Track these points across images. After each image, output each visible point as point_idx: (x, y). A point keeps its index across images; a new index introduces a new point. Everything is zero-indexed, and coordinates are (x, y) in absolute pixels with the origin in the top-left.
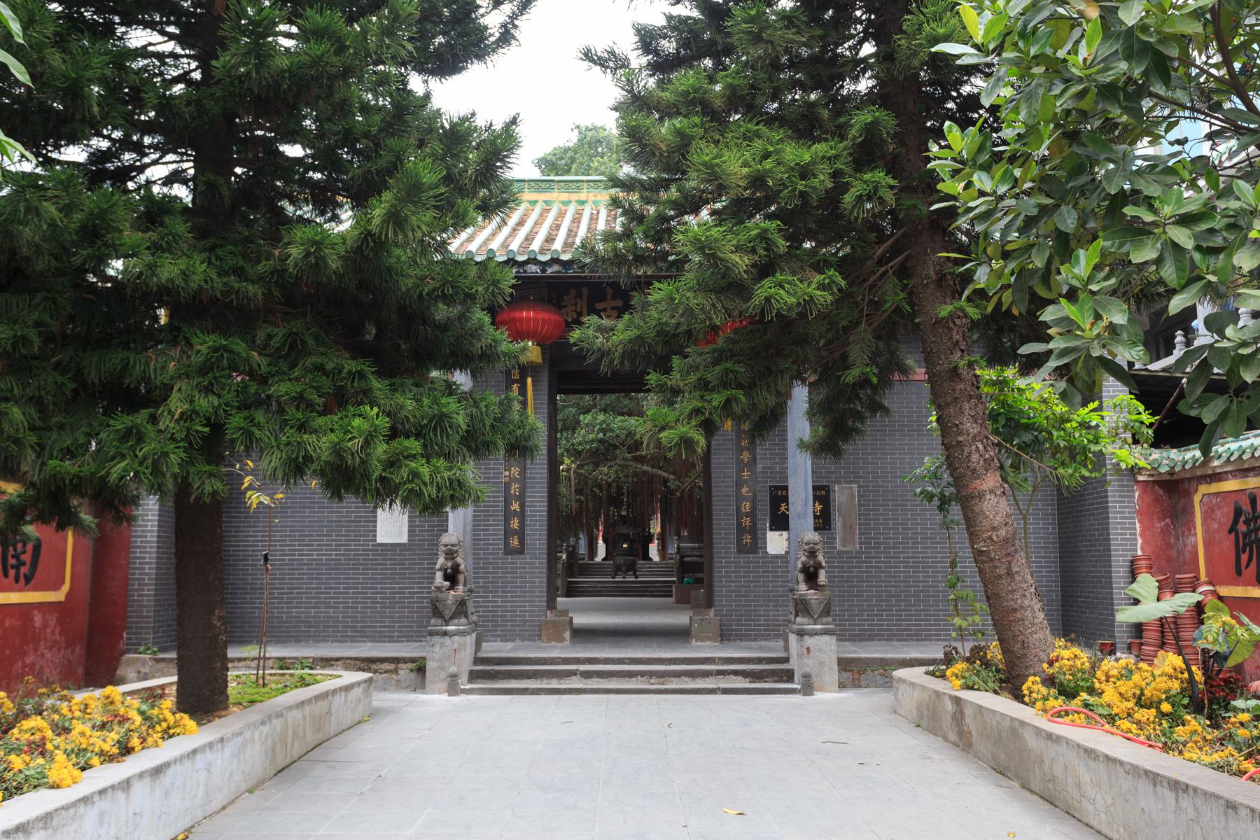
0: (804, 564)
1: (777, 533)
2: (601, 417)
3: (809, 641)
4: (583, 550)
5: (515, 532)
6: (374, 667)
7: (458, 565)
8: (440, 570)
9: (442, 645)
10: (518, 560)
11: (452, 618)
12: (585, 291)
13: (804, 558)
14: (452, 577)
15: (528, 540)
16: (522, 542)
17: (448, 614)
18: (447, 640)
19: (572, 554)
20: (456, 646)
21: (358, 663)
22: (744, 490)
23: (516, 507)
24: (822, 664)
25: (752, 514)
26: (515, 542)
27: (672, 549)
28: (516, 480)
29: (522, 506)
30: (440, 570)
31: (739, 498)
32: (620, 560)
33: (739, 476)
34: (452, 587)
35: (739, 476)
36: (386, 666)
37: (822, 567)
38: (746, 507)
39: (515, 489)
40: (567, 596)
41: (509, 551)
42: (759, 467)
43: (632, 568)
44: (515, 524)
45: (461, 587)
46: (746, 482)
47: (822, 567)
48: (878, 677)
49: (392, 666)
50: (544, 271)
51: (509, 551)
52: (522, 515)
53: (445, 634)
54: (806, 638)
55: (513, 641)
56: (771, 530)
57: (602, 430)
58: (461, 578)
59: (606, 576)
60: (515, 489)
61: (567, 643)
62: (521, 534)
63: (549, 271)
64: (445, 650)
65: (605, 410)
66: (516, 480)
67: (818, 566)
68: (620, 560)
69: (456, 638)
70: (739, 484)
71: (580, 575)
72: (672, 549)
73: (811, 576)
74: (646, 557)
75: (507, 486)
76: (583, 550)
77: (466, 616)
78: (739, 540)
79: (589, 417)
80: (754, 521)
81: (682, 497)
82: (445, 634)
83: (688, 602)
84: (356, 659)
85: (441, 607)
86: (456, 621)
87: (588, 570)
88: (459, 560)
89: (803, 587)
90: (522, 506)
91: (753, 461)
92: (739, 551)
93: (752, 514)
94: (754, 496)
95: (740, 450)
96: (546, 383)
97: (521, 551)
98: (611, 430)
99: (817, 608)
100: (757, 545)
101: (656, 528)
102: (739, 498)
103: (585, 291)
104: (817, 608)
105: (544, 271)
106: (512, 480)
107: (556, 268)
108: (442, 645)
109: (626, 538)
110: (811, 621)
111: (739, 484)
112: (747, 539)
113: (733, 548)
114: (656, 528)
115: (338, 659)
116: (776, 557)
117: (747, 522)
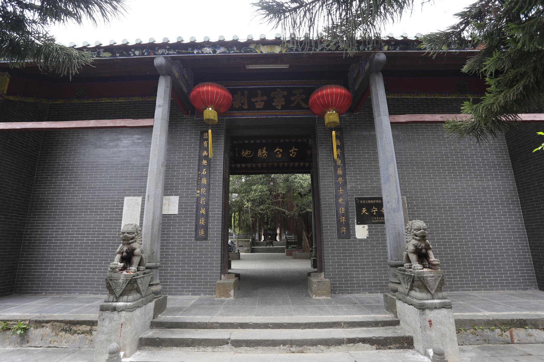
0: (416, 246)
1: (361, 226)
2: (260, 186)
3: (431, 315)
4: (257, 238)
5: (202, 227)
6: (74, 328)
7: (133, 250)
8: (119, 253)
9: (111, 320)
10: (203, 243)
11: (122, 295)
12: (246, 92)
13: (414, 242)
14: (127, 259)
15: (210, 231)
16: (206, 233)
17: (119, 291)
18: (115, 315)
19: (254, 239)
20: (123, 320)
21: (63, 325)
22: (340, 200)
23: (203, 211)
24: (443, 335)
25: (346, 214)
26: (202, 232)
27: (284, 237)
28: (204, 196)
29: (207, 211)
30: (119, 253)
31: (337, 205)
32: (268, 241)
33: (337, 192)
34: (124, 269)
35: (337, 192)
36: (84, 328)
37: (430, 249)
38: (342, 210)
39: (203, 201)
40: (252, 252)
41: (197, 238)
42: (349, 187)
43: (271, 244)
44: (202, 222)
45: (133, 268)
46: (341, 196)
47: (430, 249)
48: (471, 336)
49: (88, 328)
50: (214, 52)
51: (197, 238)
52: (207, 216)
53: (114, 309)
54: (427, 311)
55: (199, 294)
56: (358, 224)
57: (260, 192)
58: (136, 260)
59: (264, 246)
60: (203, 201)
61: (232, 298)
62: (206, 228)
63: (218, 51)
64: (114, 324)
65: (262, 184)
66: (204, 196)
67: (427, 248)
68: (268, 241)
69: (124, 313)
70: (337, 197)
71: (256, 246)
72: (284, 237)
73: (422, 256)
74: (276, 240)
75: (198, 199)
76: (257, 238)
77: (138, 291)
78: (339, 230)
79: (255, 187)
80: (347, 219)
81: (291, 217)
82: (114, 309)
83: (291, 255)
84: (61, 322)
85: (113, 286)
86: (125, 297)
87: (258, 244)
88: (135, 245)
89: (417, 266)
90: (207, 211)
91: (345, 183)
92: (339, 238)
93: (346, 214)
94: (347, 204)
95: (338, 176)
96: (223, 141)
97: (205, 238)
98: (264, 191)
99: (434, 285)
100: (349, 234)
101: (278, 232)
102: (337, 205)
103: (246, 92)
104: (434, 285)
105: (214, 52)
106: (201, 195)
107: (222, 49)
108: (111, 320)
109: (270, 234)
110: (429, 296)
111: (337, 197)
112: (344, 230)
113: (335, 235)
114: (278, 232)
115: (48, 322)
116: (361, 240)
117: (343, 219)
